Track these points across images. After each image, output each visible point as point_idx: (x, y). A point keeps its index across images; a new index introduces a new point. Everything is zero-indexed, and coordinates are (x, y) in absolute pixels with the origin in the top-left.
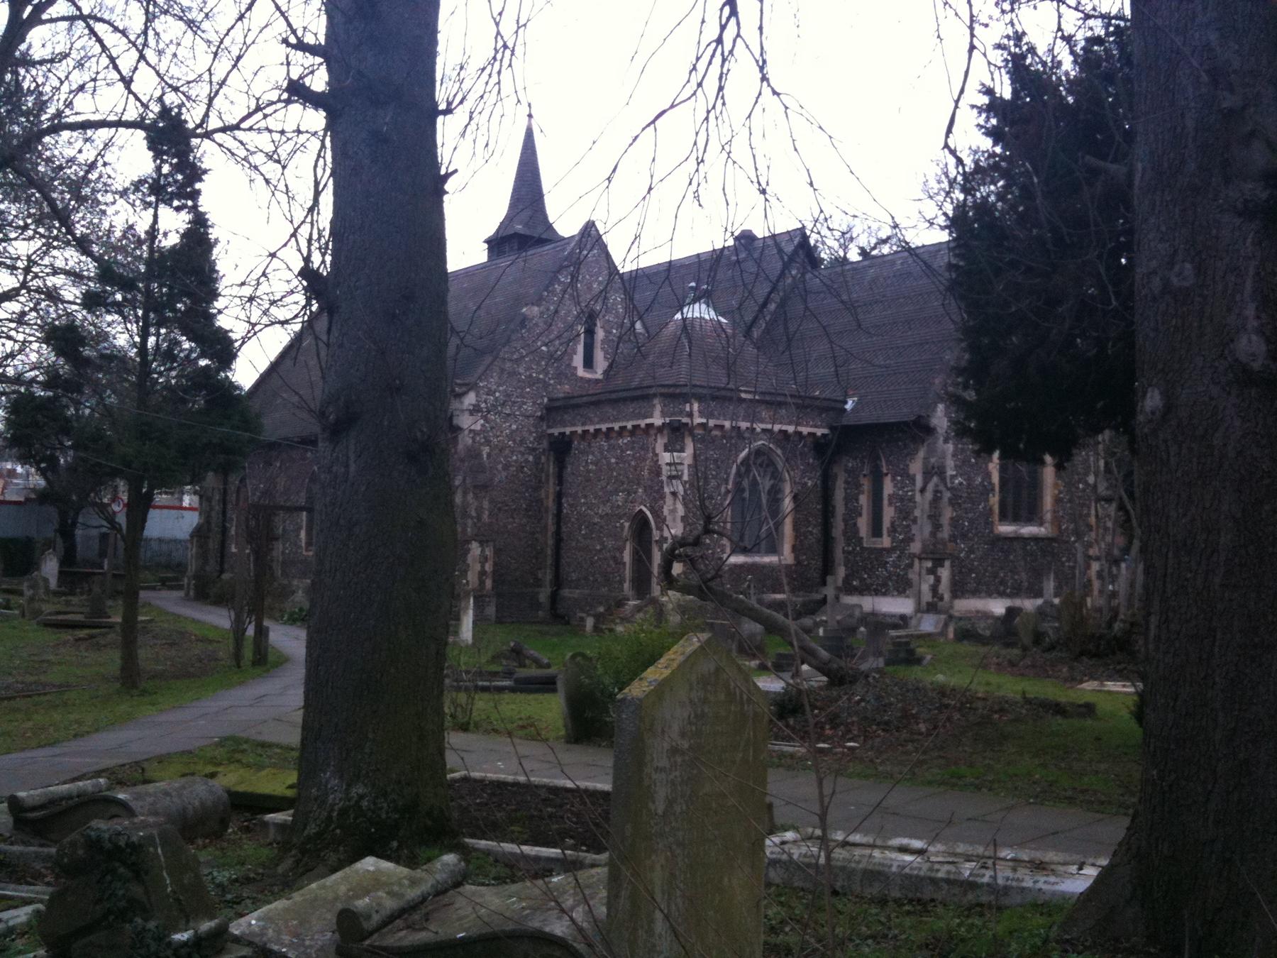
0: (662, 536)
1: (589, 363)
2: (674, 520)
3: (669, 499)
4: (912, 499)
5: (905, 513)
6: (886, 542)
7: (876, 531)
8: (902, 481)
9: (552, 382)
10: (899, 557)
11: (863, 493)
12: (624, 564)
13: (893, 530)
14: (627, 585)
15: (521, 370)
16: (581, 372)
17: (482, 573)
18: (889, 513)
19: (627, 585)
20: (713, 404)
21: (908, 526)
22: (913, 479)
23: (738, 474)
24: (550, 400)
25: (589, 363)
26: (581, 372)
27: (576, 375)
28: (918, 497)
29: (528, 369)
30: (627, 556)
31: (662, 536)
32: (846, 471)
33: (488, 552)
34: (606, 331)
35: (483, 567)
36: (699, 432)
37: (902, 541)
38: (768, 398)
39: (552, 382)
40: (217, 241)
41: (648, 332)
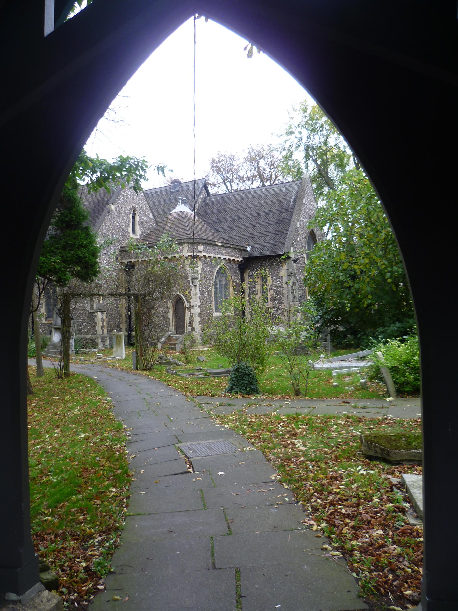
0: (190, 305)
1: (134, 232)
2: (196, 298)
3: (193, 288)
4: (281, 286)
5: (278, 292)
6: (270, 304)
7: (265, 299)
8: (276, 279)
9: (121, 239)
10: (277, 310)
11: (258, 284)
12: (169, 319)
13: (273, 299)
14: (171, 328)
15: (109, 234)
16: (132, 235)
17: (103, 327)
18: (271, 293)
19: (171, 328)
20: (207, 247)
21: (280, 297)
22: (281, 278)
23: (216, 278)
24: (121, 247)
25: (134, 232)
26: (132, 235)
27: (129, 236)
28: (285, 285)
29: (112, 233)
30: (171, 315)
31: (190, 305)
32: (249, 276)
33: (104, 317)
34: (140, 218)
35: (103, 324)
36: (203, 259)
37: (278, 303)
38: (224, 245)
39: (121, 239)
40: (259, 52)
41: (155, 218)
